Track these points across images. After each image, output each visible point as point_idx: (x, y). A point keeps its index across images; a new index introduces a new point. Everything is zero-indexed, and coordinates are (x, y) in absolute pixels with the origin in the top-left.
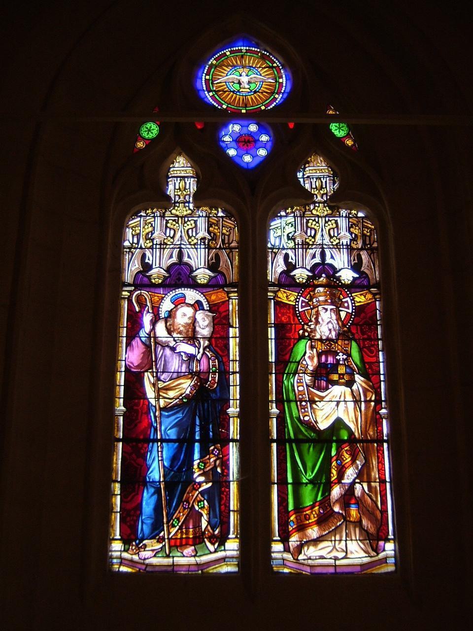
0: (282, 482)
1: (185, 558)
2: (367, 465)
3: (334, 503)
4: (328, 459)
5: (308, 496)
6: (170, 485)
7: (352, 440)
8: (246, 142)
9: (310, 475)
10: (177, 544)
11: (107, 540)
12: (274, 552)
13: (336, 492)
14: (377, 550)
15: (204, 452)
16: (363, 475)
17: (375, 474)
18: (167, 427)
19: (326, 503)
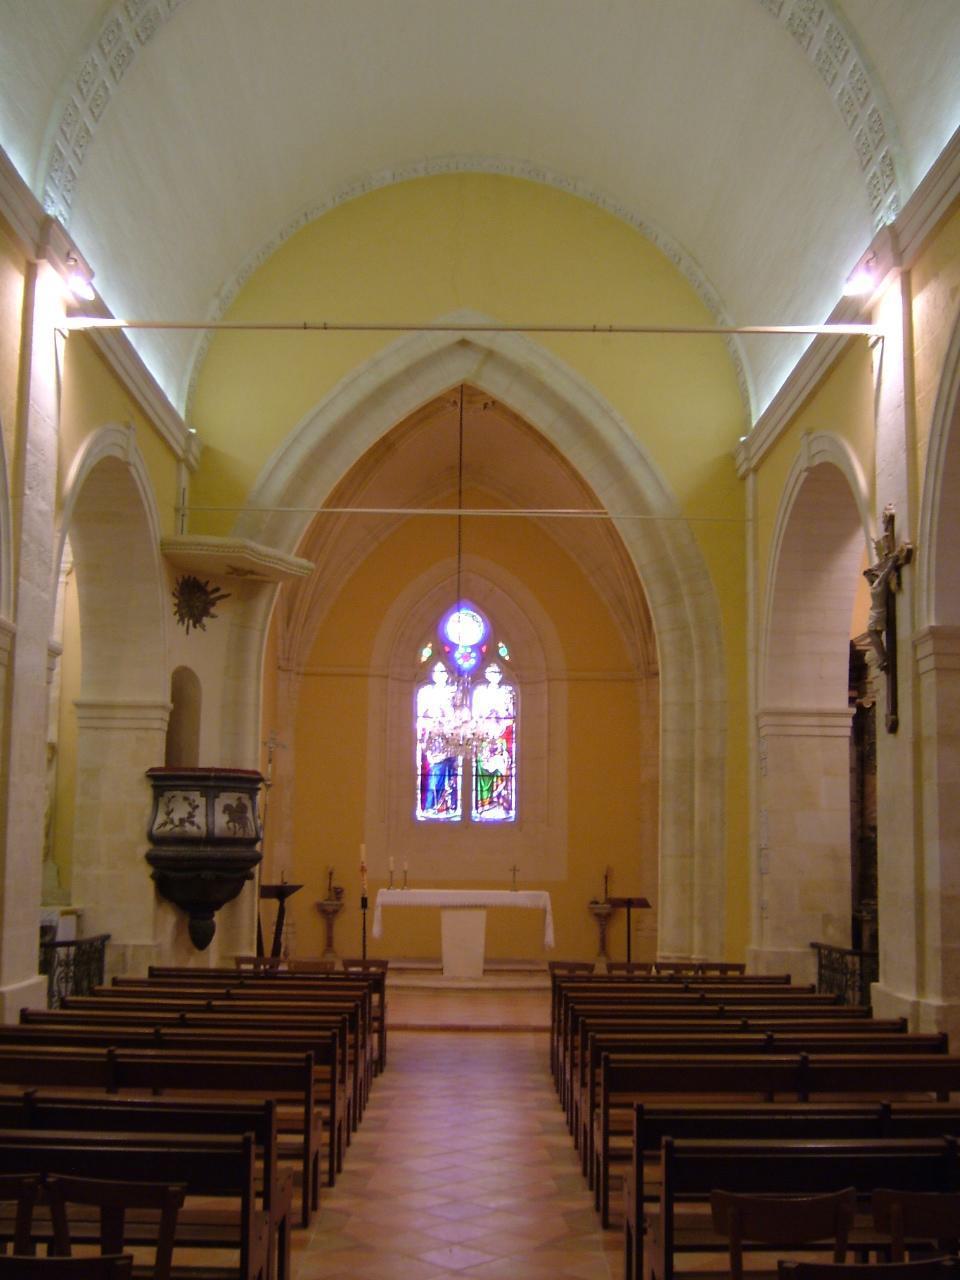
0: (477, 790)
1: (443, 816)
2: (506, 785)
3: (255, 1179)
4: (493, 782)
5: (485, 794)
6: (437, 791)
7: (502, 776)
8: (466, 657)
9: (487, 788)
10: (440, 811)
11: (415, 809)
12: (71, 1221)
13: (495, 794)
14: (508, 813)
15: (449, 779)
16: (505, 788)
17: (509, 788)
18: (435, 771)
19: (491, 797)
